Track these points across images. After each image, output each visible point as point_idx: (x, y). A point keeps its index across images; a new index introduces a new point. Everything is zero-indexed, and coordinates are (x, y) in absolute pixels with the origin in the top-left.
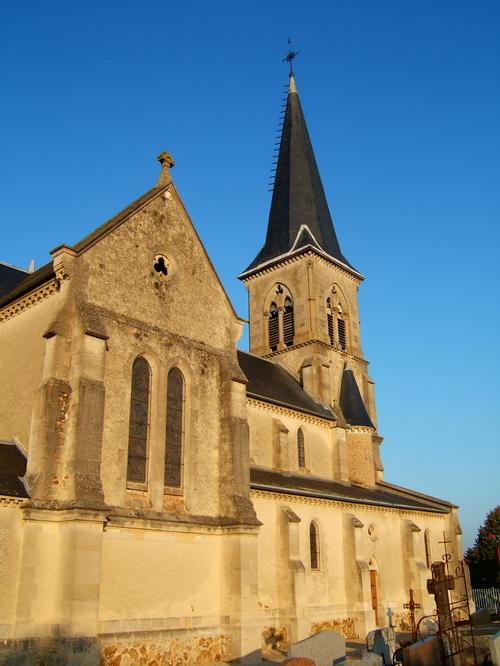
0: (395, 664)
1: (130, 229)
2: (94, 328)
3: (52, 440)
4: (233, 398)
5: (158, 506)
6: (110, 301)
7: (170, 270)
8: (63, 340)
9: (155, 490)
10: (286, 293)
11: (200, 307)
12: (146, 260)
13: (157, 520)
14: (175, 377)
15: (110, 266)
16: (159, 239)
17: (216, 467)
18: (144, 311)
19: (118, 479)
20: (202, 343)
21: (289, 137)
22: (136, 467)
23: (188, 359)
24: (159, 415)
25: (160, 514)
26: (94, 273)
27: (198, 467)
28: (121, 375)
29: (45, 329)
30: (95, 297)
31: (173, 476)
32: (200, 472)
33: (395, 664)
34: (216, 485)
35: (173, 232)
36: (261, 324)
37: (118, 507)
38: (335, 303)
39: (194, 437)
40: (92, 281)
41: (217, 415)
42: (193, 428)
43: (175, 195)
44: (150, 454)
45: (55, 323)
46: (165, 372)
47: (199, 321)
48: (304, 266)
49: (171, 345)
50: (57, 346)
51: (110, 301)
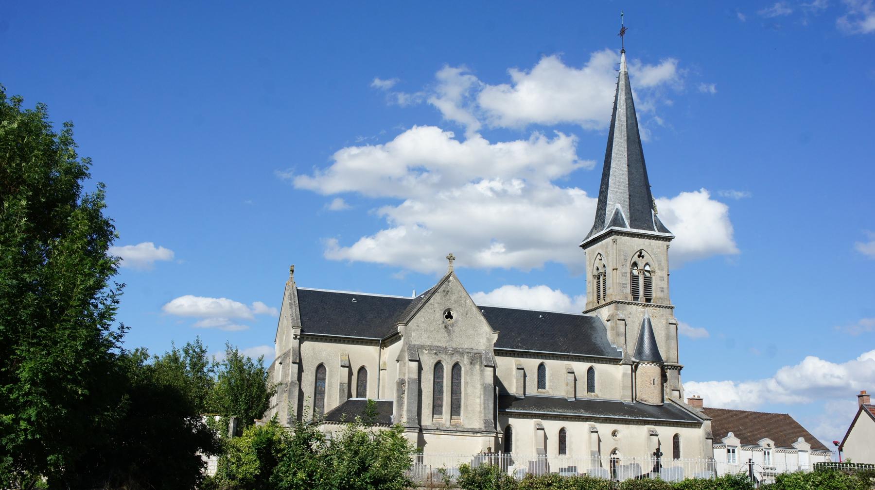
0: (474, 489)
1: (431, 304)
2: (413, 357)
3: (400, 398)
4: (485, 374)
5: (448, 424)
6: (423, 341)
7: (454, 316)
8: (402, 362)
9: (445, 419)
10: (603, 262)
11: (471, 331)
12: (439, 315)
13: (447, 431)
14: (456, 367)
15: (422, 325)
16: (446, 303)
17: (478, 406)
18: (439, 341)
19: (429, 415)
20: (472, 349)
21: (615, 121)
22: (437, 409)
23: (462, 359)
24: (447, 386)
25: (448, 428)
26: (414, 331)
27: (468, 407)
28: (428, 372)
29: (396, 358)
30: (415, 341)
31: (455, 409)
32: (469, 409)
33: (474, 489)
34: (478, 414)
35: (454, 298)
36: (591, 282)
37: (429, 426)
38: (641, 263)
39: (466, 394)
40: (413, 334)
41: (479, 383)
42: (465, 390)
43: (455, 277)
44: (444, 403)
45: (399, 356)
46: (450, 367)
47: (470, 338)
48: (611, 242)
49: (453, 354)
50: (400, 365)
51: (423, 341)
